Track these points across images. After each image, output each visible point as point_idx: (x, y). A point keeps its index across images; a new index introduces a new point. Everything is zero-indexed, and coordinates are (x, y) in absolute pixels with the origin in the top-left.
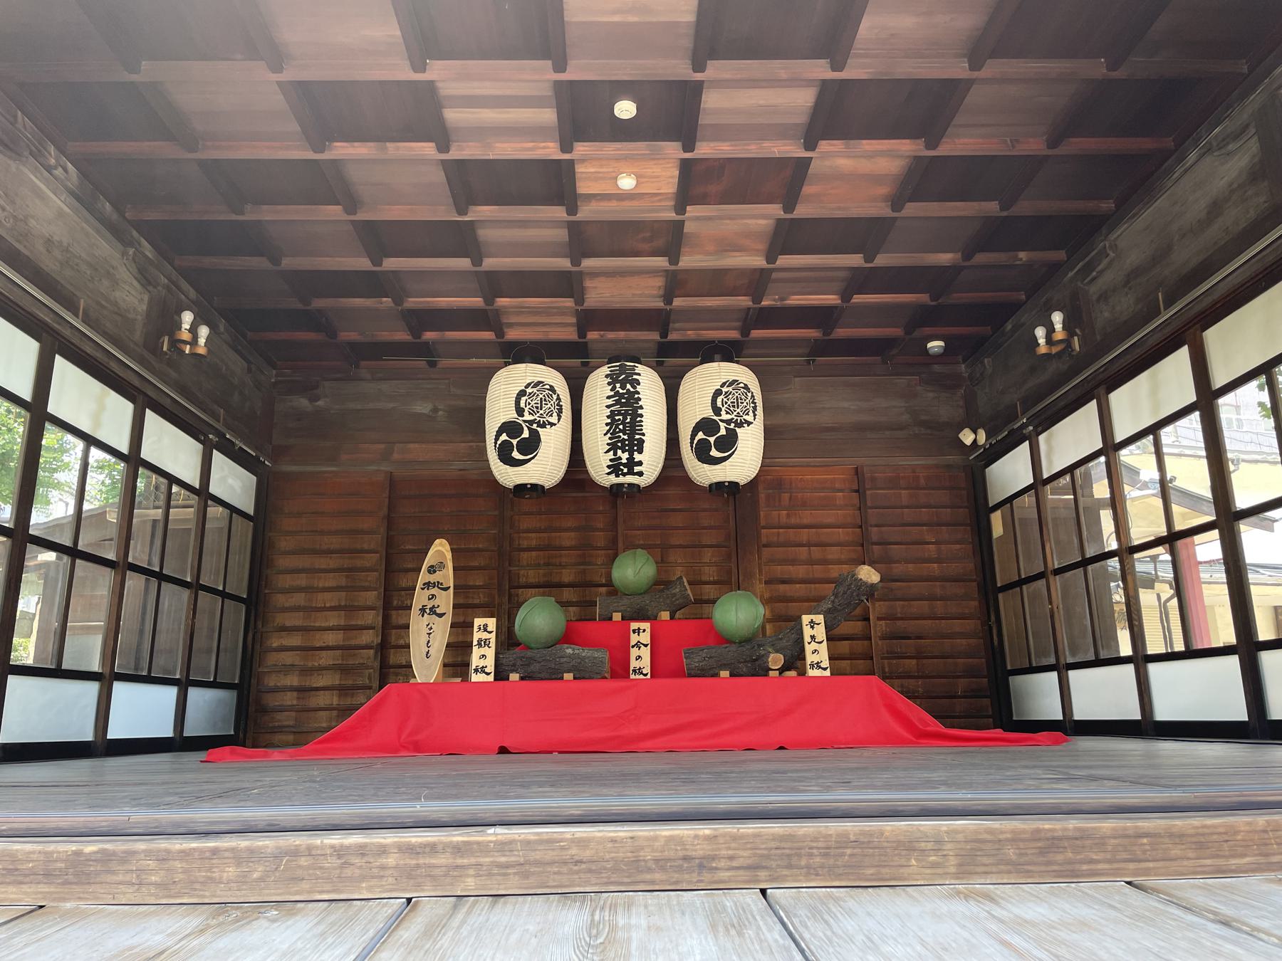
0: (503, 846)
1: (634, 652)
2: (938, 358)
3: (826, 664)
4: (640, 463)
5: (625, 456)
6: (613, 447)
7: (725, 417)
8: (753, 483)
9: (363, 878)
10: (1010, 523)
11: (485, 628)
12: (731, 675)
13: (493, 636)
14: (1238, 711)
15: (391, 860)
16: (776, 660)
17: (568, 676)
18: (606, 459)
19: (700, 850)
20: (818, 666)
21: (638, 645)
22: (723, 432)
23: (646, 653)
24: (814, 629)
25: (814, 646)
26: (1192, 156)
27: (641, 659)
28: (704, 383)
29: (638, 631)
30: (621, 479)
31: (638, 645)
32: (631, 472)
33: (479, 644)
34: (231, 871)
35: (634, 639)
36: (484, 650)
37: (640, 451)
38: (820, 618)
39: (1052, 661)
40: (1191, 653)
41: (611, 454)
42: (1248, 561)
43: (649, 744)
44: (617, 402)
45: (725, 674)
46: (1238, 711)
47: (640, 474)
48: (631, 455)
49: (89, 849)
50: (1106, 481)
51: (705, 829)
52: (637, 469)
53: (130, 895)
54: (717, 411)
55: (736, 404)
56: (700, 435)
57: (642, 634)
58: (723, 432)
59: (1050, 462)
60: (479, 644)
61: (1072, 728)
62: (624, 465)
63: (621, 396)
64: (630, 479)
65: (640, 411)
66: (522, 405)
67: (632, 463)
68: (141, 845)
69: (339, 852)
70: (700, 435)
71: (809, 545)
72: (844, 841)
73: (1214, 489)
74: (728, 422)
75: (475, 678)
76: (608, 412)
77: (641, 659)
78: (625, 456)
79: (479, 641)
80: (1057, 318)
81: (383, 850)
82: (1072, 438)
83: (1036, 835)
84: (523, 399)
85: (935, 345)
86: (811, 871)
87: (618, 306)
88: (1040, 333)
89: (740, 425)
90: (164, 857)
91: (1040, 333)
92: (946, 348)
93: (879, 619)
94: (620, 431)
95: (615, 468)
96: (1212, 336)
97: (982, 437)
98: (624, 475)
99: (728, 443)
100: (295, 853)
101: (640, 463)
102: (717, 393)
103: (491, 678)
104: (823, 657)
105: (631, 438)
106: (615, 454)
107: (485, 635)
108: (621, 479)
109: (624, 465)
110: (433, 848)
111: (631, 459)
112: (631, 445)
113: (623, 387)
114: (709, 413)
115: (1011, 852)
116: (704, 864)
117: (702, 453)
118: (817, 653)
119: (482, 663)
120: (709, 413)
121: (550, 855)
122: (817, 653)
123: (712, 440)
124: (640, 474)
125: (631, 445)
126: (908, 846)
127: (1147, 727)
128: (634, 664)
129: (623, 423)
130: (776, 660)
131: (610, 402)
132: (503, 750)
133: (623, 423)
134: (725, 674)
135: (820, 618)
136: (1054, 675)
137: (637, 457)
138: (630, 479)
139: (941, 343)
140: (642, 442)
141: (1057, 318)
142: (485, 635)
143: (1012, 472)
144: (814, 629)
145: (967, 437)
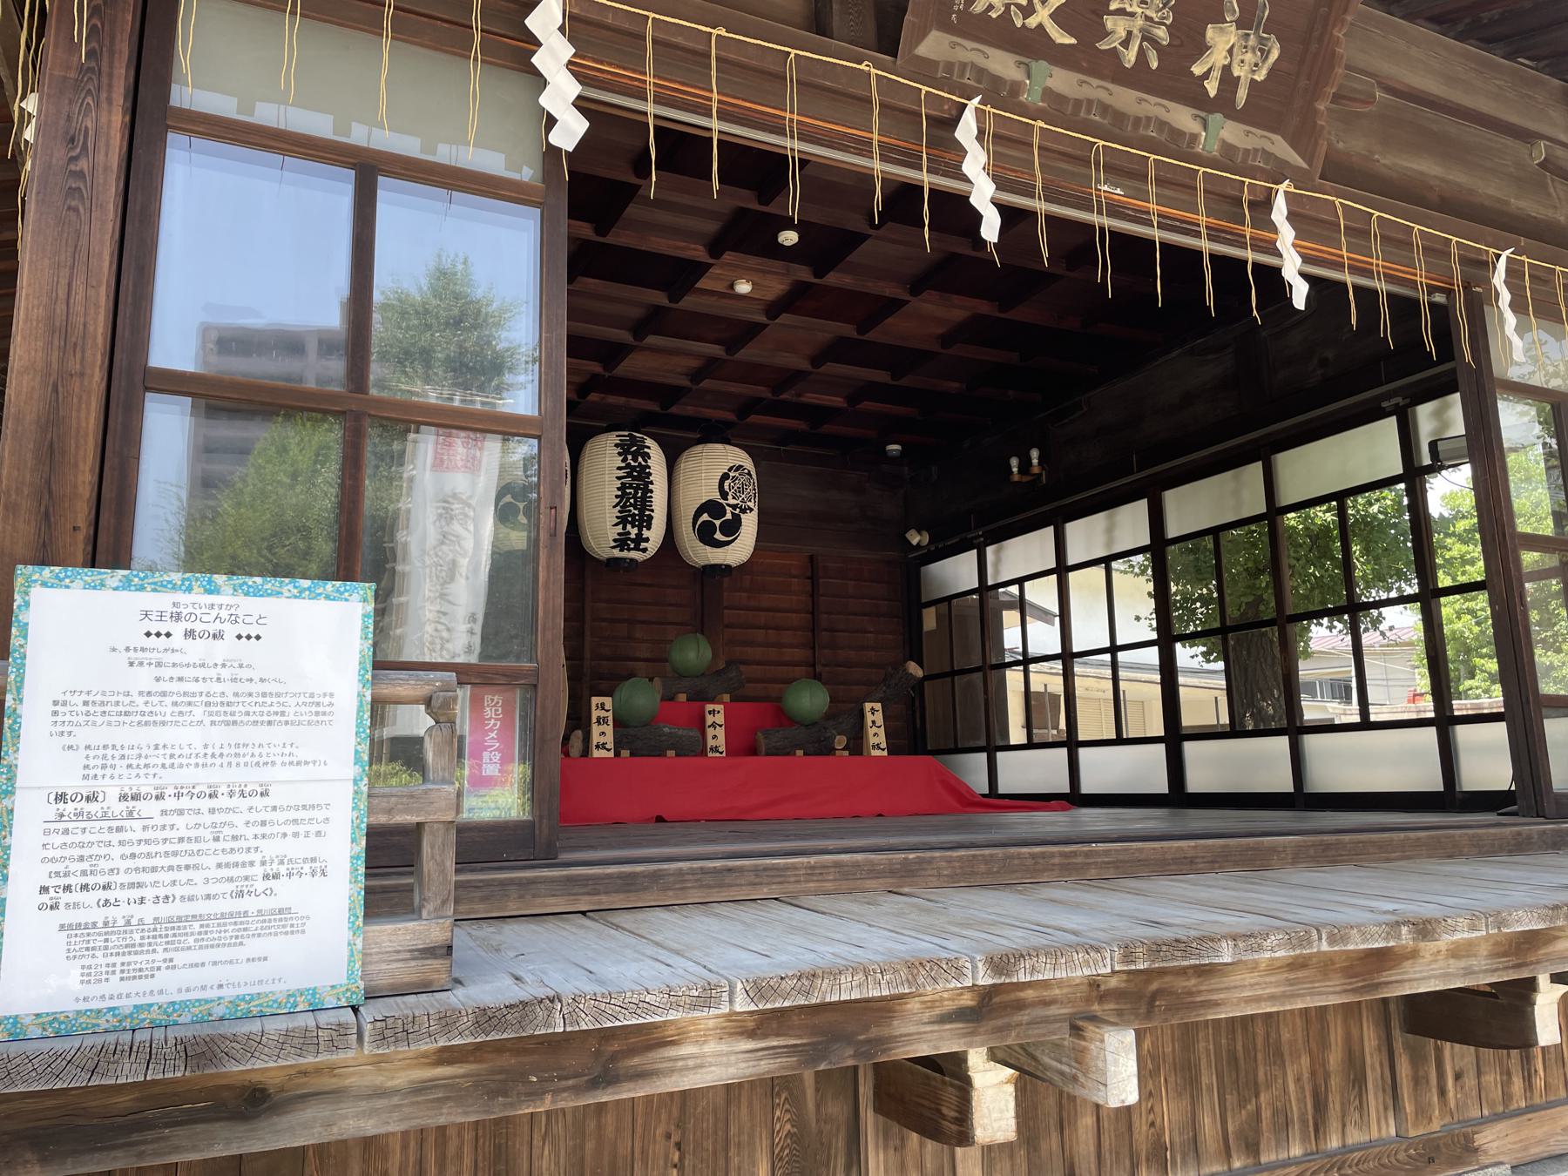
0: (1107, 853)
1: (710, 732)
2: (893, 460)
3: (884, 745)
4: (647, 540)
5: (634, 531)
6: (623, 521)
7: (732, 501)
8: (742, 567)
9: (1045, 870)
10: (946, 620)
11: (601, 707)
12: (677, 755)
13: (610, 714)
14: (1161, 785)
15: (1056, 860)
16: (840, 741)
17: (671, 753)
18: (614, 532)
19: (1191, 853)
20: (878, 746)
21: (714, 725)
22: (729, 516)
23: (721, 732)
24: (874, 714)
25: (875, 730)
26: (1174, 354)
27: (717, 738)
28: (713, 468)
29: (713, 712)
30: (625, 554)
31: (714, 725)
32: (637, 548)
33: (598, 722)
34: (983, 868)
35: (710, 719)
36: (603, 728)
37: (649, 528)
38: (878, 706)
39: (983, 743)
40: (1120, 741)
42: (1007, 646)
43: (761, 814)
44: (629, 475)
45: (800, 753)
46: (1161, 785)
47: (645, 550)
48: (640, 530)
49: (911, 856)
51: (1192, 843)
52: (643, 545)
53: (934, 881)
54: (724, 495)
55: (741, 490)
56: (705, 517)
57: (716, 715)
58: (729, 516)
59: (997, 572)
60: (598, 722)
61: (998, 801)
62: (633, 540)
63: (628, 466)
64: (634, 555)
67: (640, 539)
68: (937, 854)
69: (1033, 856)
70: (705, 517)
71: (767, 628)
72: (1248, 848)
74: (734, 507)
75: (597, 754)
76: (618, 484)
77: (717, 738)
78: (634, 531)
79: (598, 719)
80: (1035, 454)
81: (1052, 855)
82: (1025, 553)
83: (1321, 843)
85: (894, 448)
86: (1236, 863)
87: (645, 378)
88: (1014, 462)
89: (744, 511)
90: (949, 861)
91: (1014, 462)
92: (902, 452)
95: (622, 543)
96: (1171, 498)
97: (926, 539)
98: (629, 550)
99: (733, 527)
100: (1012, 857)
101: (647, 540)
102: (725, 477)
103: (611, 754)
104: (882, 739)
107: (603, 714)
108: (625, 554)
109: (633, 540)
110: (1074, 854)
111: (639, 535)
112: (641, 521)
113: (635, 460)
114: (716, 496)
115: (1312, 852)
116: (1192, 861)
117: (706, 535)
118: (876, 736)
119: (602, 740)
120: (716, 496)
121: (1126, 858)
122: (876, 736)
123: (718, 523)
124: (645, 550)
126: (1273, 850)
127: (1075, 798)
128: (711, 743)
129: (635, 497)
130: (840, 741)
131: (621, 473)
132: (660, 819)
133: (635, 497)
134: (800, 753)
135: (878, 706)
136: (984, 755)
138: (634, 555)
139: (897, 447)
141: (1035, 454)
142: (603, 714)
143: (959, 572)
144: (874, 714)
145: (915, 538)
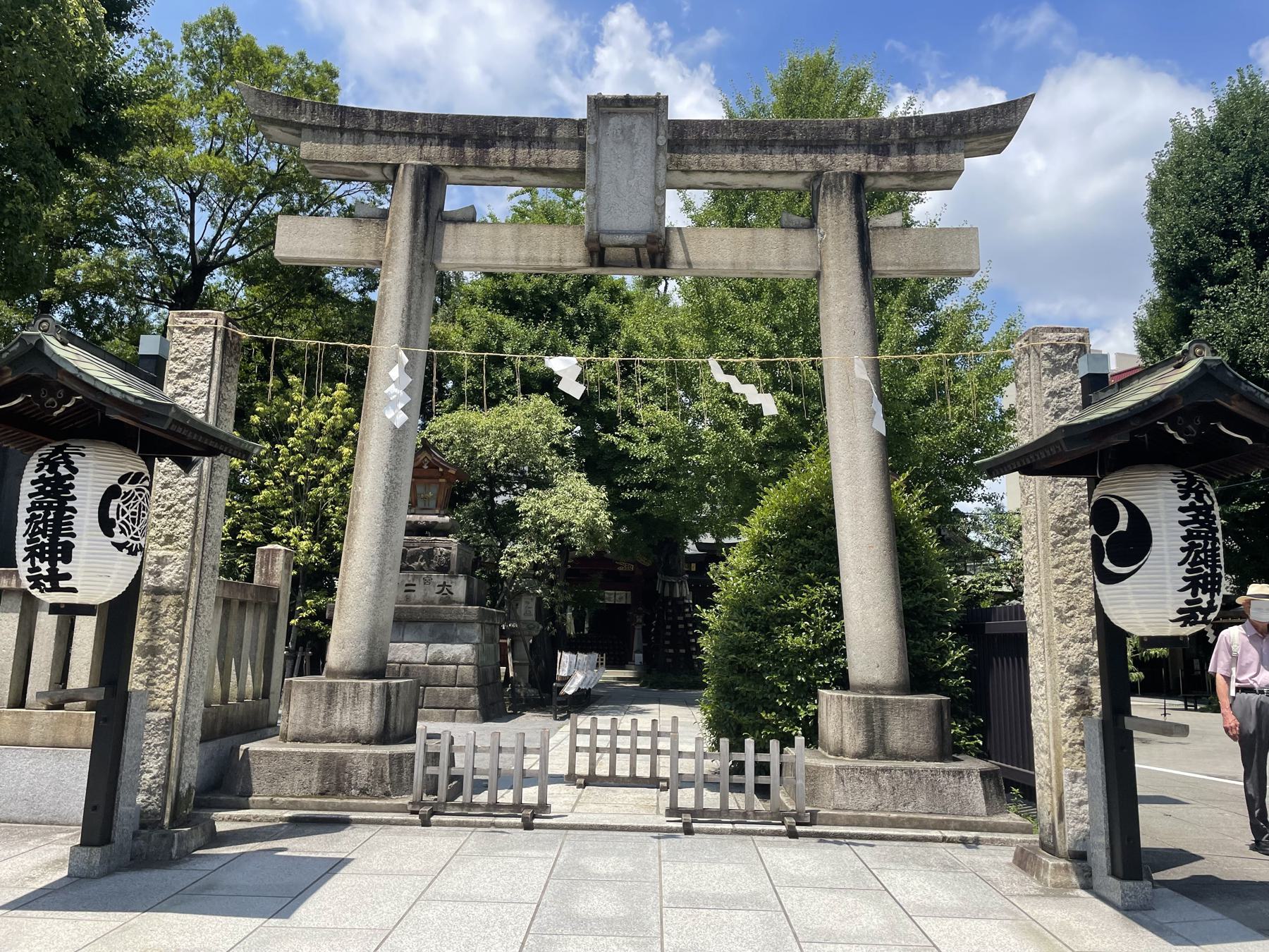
4: (67, 577)
5: (44, 567)
32: (55, 588)
37: (67, 559)
41: (1188, 595)
50: (476, 189)
62: (46, 579)
65: (1185, 517)
66: (112, 514)
73: (91, 806)
76: (1183, 531)
78: (44, 567)
84: (114, 503)
93: (675, 719)
94: (1202, 562)
101: (67, 577)
105: (53, 539)
106: (33, 563)
111: (53, 570)
112: (53, 552)
125: (53, 552)
129: (45, 521)
137: (62, 568)
140: (69, 547)
